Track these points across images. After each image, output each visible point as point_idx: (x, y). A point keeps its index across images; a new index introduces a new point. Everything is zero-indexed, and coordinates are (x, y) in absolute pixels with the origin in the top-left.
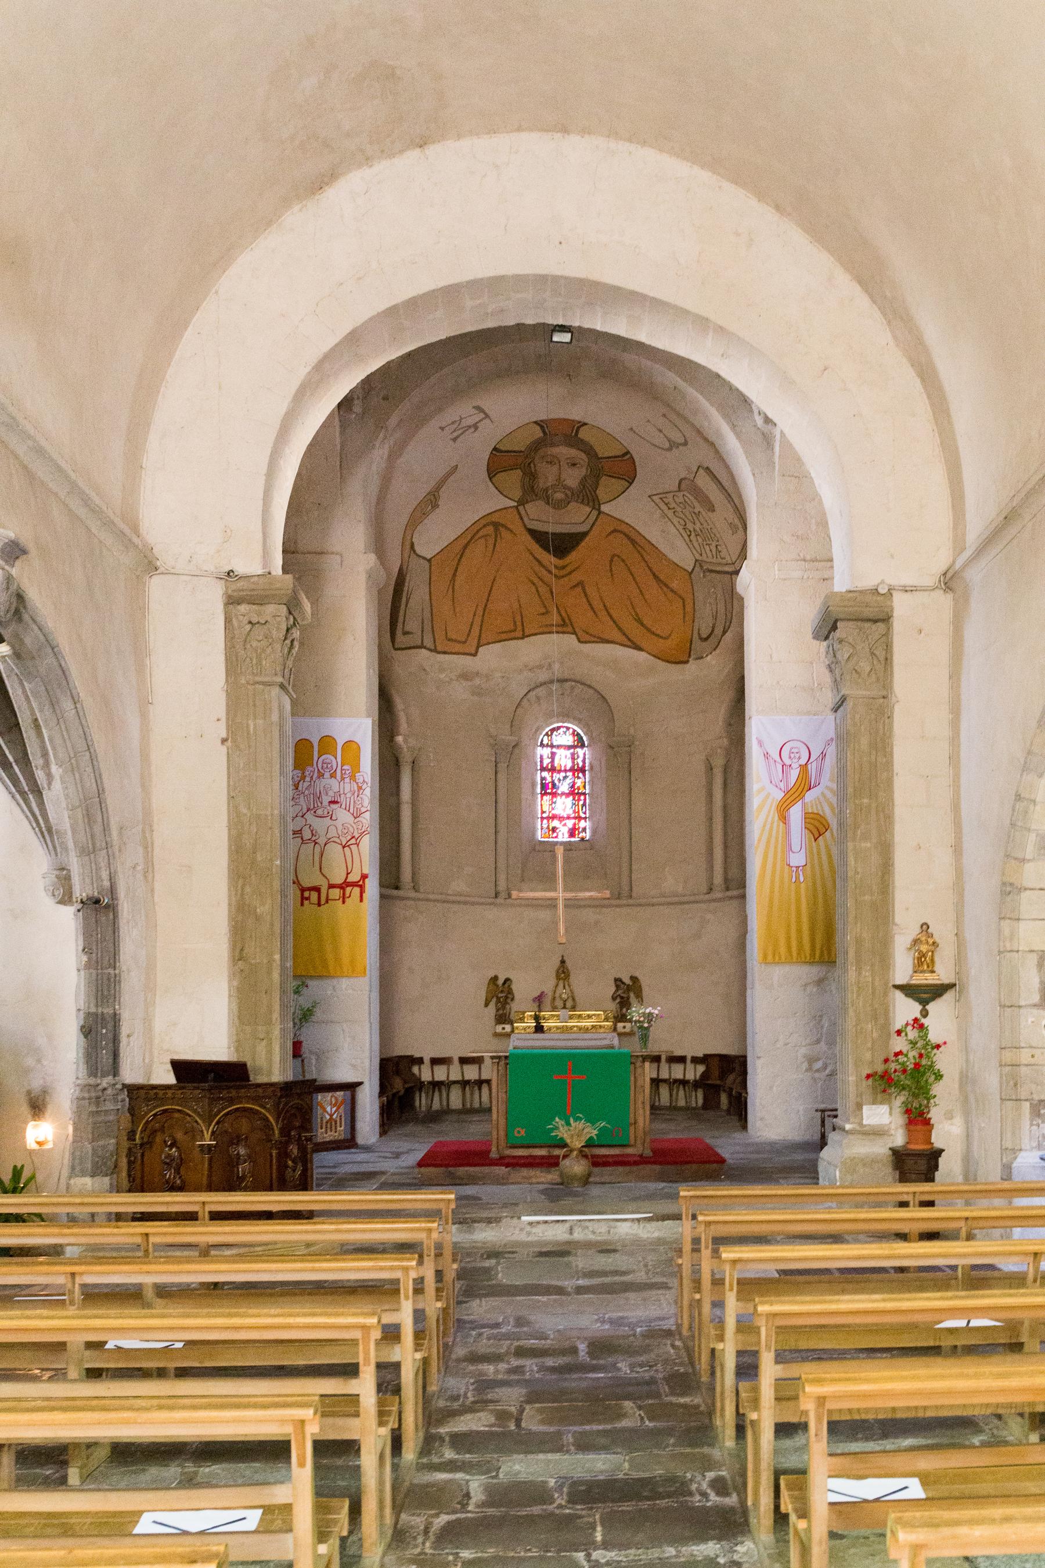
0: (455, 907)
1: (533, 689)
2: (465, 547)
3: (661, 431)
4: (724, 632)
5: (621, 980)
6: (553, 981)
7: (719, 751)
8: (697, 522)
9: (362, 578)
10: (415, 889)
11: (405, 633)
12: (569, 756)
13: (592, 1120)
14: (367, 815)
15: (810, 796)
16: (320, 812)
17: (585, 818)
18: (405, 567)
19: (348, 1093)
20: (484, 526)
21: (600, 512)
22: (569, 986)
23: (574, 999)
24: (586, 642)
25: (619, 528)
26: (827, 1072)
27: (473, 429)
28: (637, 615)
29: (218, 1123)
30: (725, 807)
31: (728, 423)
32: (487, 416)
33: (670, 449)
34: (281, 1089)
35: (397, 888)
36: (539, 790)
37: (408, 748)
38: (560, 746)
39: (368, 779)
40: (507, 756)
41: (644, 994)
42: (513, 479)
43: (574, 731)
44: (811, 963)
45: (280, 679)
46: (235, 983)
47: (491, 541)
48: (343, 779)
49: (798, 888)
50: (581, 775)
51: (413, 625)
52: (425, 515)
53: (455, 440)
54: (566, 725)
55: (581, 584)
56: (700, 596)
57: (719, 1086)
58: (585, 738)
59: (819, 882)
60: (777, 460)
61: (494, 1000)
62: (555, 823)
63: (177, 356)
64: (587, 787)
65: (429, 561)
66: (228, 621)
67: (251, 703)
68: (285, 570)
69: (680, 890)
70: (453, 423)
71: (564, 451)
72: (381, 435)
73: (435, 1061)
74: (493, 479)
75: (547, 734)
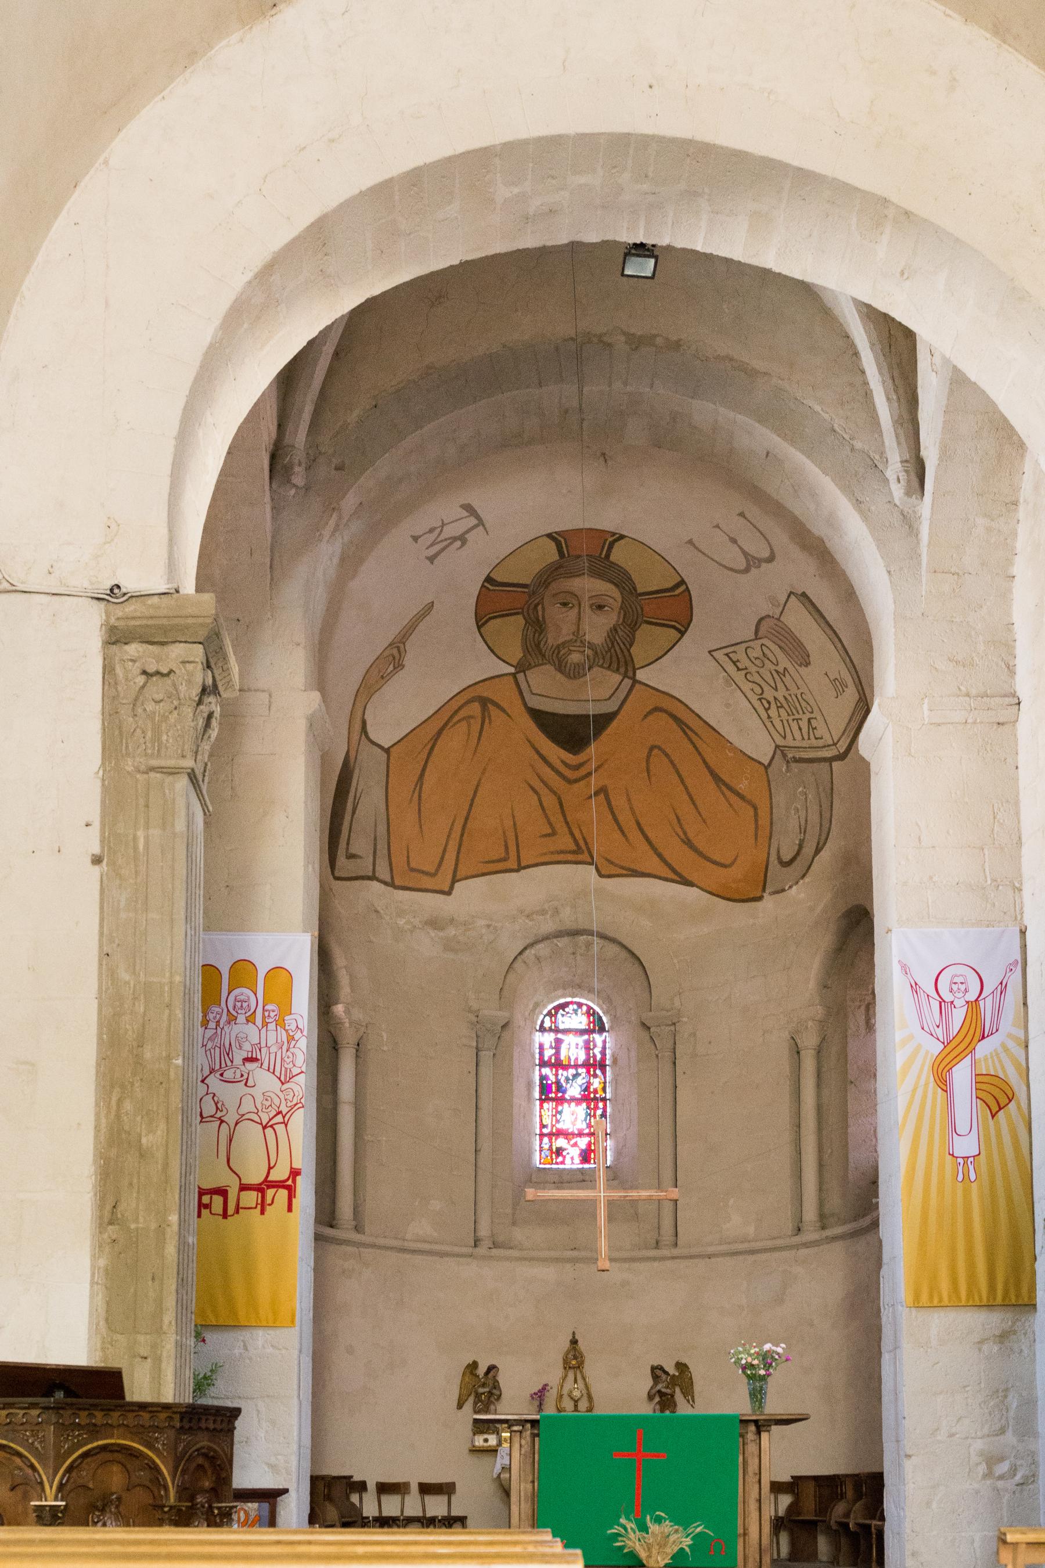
0: (418, 1259)
1: (531, 945)
2: (439, 733)
3: (734, 541)
4: (818, 851)
5: (661, 1368)
6: (559, 1372)
7: (810, 1023)
8: (780, 685)
9: (302, 725)
10: (358, 1228)
11: (351, 856)
12: (581, 1044)
13: (683, 1521)
14: (301, 1079)
15: (983, 1049)
16: (229, 1075)
19: (266, 1506)
21: (635, 682)
22: (584, 1379)
23: (590, 1398)
24: (609, 876)
25: (664, 705)
26: (1018, 1478)
27: (458, 543)
28: (685, 833)
29: (70, 1469)
30: (819, 1108)
31: (850, 500)
32: (481, 522)
33: (747, 570)
34: (183, 1416)
35: (332, 1226)
36: (537, 1095)
37: (350, 1023)
38: (566, 1030)
39: (304, 1023)
40: (492, 1039)
41: (697, 1388)
42: (511, 630)
43: (589, 1008)
44: (990, 1307)
45: (188, 763)
46: (102, 1262)
47: (476, 727)
48: (265, 1024)
49: (967, 1193)
50: (598, 1072)
51: (361, 845)
52: (384, 678)
53: (431, 559)
54: (575, 1000)
56: (780, 798)
57: (814, 1523)
58: (605, 1019)
59: (999, 1183)
60: (924, 550)
61: (471, 1400)
62: (561, 1142)
63: (40, 258)
64: (608, 1090)
65: (387, 751)
66: (108, 670)
67: (142, 801)
68: (199, 589)
69: (751, 1230)
70: (431, 531)
71: (588, 586)
72: (332, 523)
73: (384, 1488)
74: (482, 630)
75: (549, 1014)
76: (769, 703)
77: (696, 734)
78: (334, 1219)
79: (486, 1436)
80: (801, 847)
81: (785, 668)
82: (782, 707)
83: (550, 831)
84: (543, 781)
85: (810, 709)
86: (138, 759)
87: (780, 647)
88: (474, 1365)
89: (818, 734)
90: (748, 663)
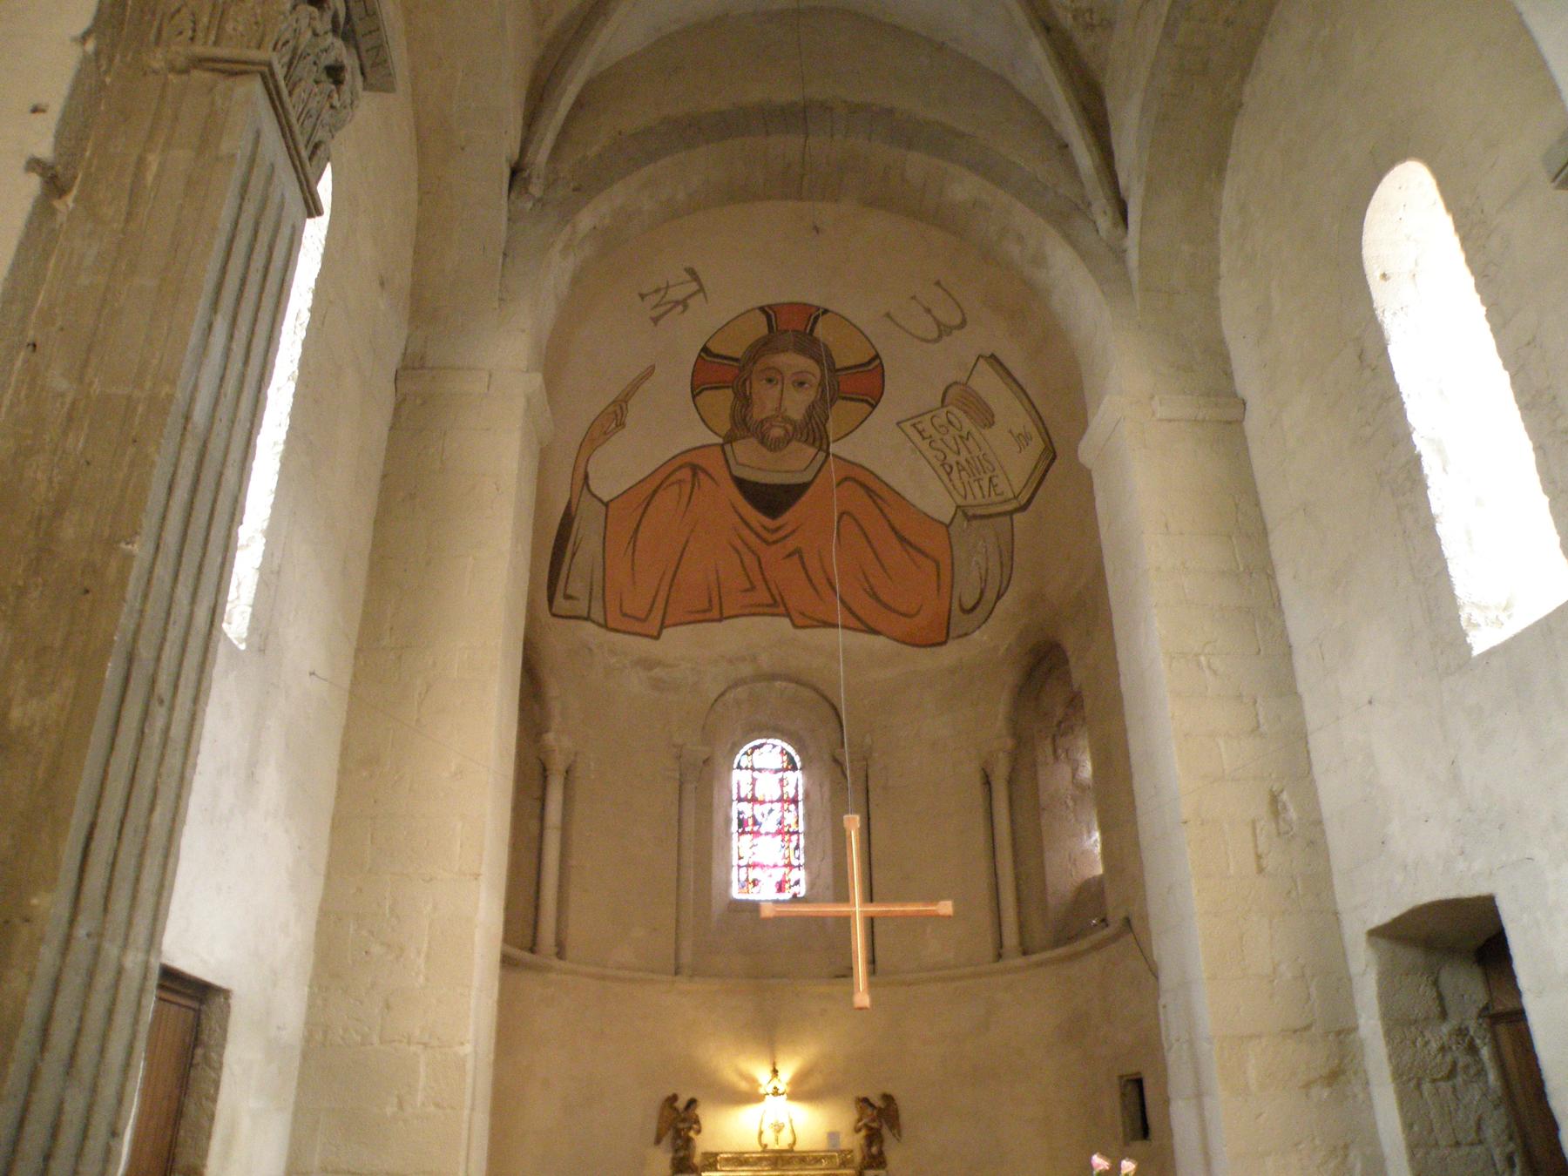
2: (655, 492)
3: (928, 311)
4: (999, 597)
7: (1001, 755)
10: (560, 954)
11: (568, 597)
18: (574, 502)
20: (680, 467)
27: (680, 308)
32: (701, 289)
38: (765, 777)
42: (721, 401)
47: (687, 489)
50: (792, 807)
51: (577, 587)
52: (607, 435)
53: (655, 320)
55: (797, 552)
58: (797, 759)
61: (671, 1133)
65: (607, 505)
70: (657, 291)
71: (792, 362)
80: (982, 593)
83: (748, 586)
86: (173, 48)
88: (674, 1098)
90: (933, 431)
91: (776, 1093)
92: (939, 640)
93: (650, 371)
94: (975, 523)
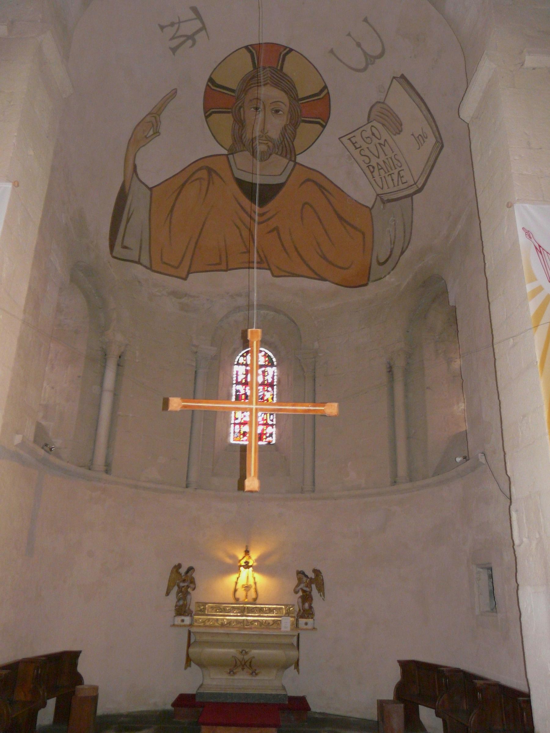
2: (183, 185)
4: (402, 253)
10: (107, 472)
17: (272, 425)
20: (200, 169)
21: (296, 163)
27: (190, 42)
32: (204, 28)
33: (365, 69)
38: (254, 369)
42: (225, 121)
43: (266, 353)
50: (270, 389)
53: (174, 50)
55: (276, 229)
58: (274, 360)
61: (176, 589)
64: (275, 399)
65: (151, 189)
70: (172, 24)
71: (269, 93)
75: (243, 356)
76: (373, 168)
77: (330, 194)
78: (92, 464)
79: (183, 618)
81: (385, 140)
82: (382, 168)
84: (242, 222)
85: (399, 164)
87: (383, 125)
88: (179, 566)
89: (404, 180)
91: (247, 566)
92: (364, 282)
93: (174, 93)
94: (388, 205)
